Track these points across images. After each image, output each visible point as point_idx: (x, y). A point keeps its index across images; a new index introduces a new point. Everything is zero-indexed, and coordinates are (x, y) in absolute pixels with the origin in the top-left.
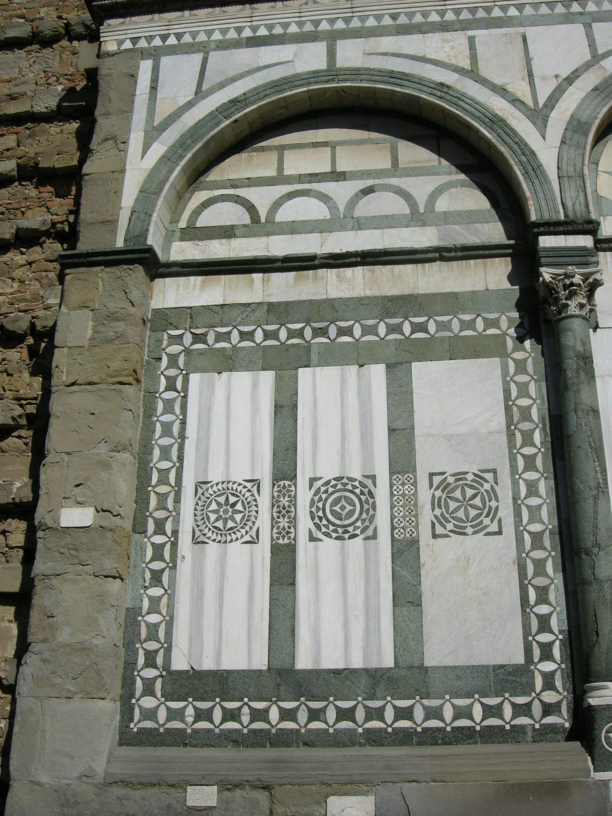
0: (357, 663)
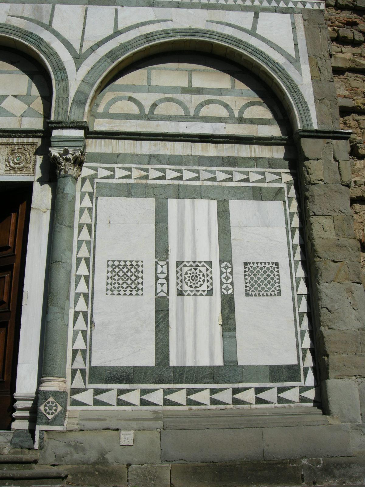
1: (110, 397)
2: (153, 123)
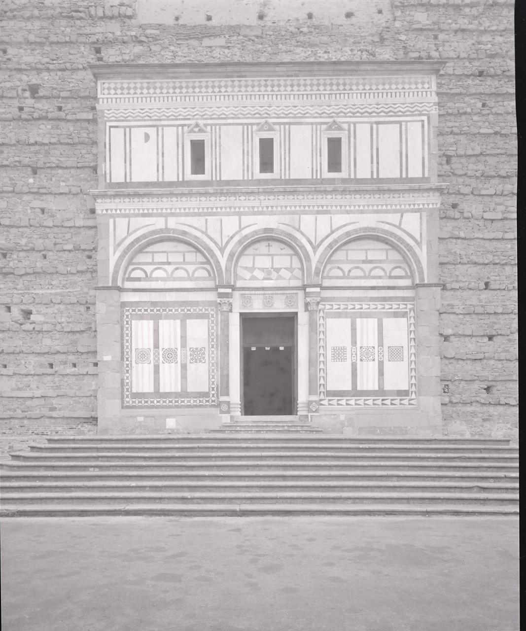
0: (173, 391)
1: (334, 402)
2: (350, 280)
